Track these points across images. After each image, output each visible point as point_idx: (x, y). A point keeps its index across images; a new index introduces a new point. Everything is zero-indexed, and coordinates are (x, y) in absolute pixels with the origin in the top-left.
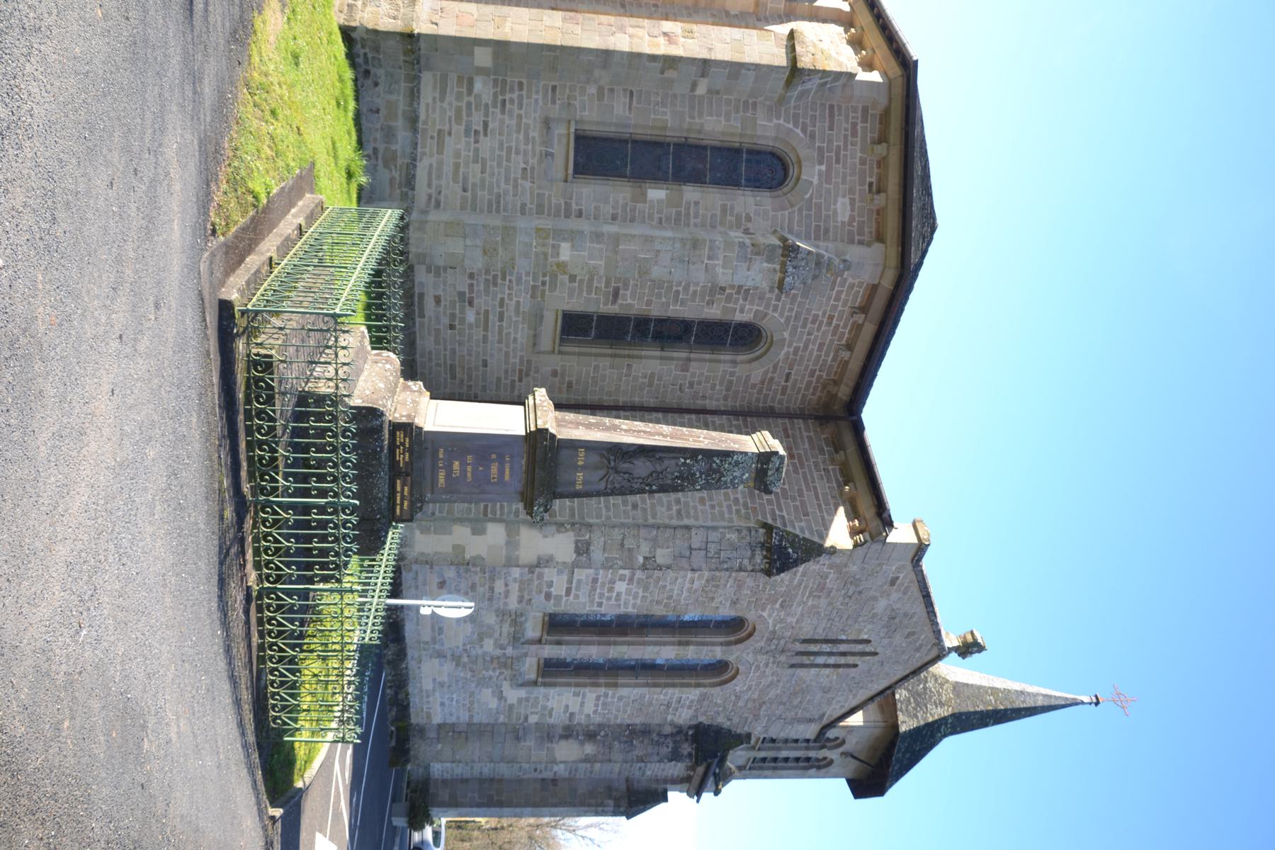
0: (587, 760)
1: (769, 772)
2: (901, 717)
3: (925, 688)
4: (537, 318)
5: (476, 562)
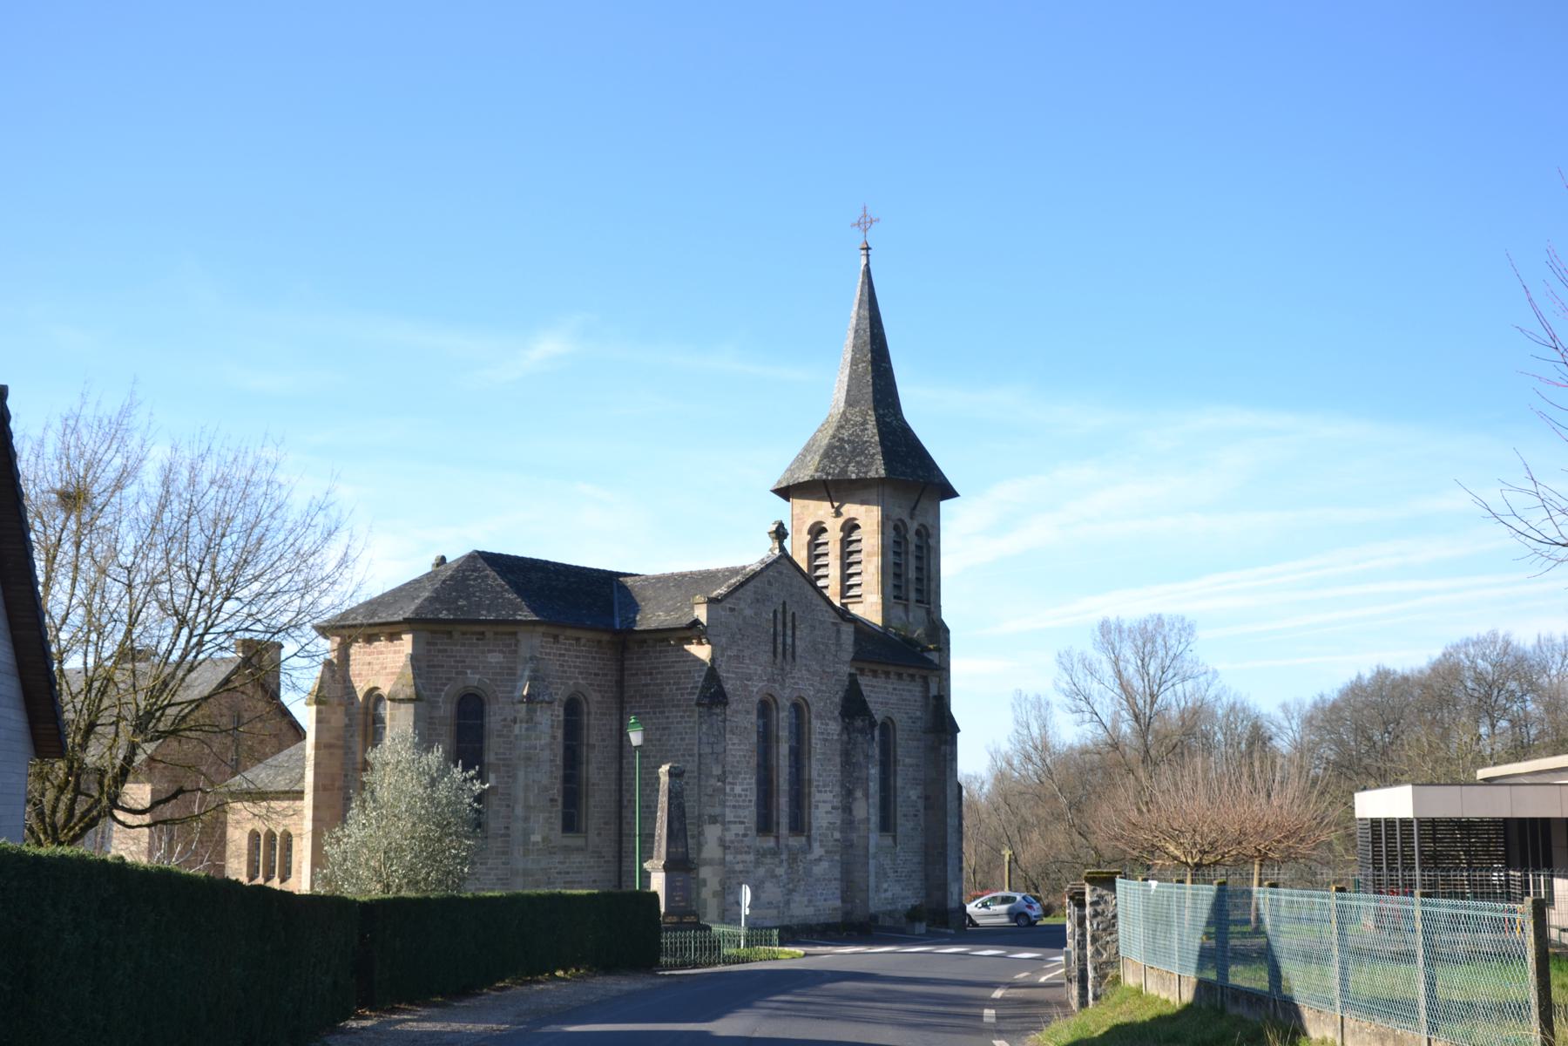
0: (867, 795)
1: (933, 585)
2: (872, 474)
3: (849, 442)
4: (567, 850)
5: (722, 883)
